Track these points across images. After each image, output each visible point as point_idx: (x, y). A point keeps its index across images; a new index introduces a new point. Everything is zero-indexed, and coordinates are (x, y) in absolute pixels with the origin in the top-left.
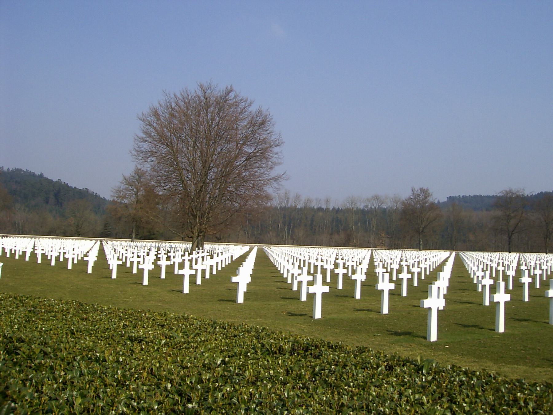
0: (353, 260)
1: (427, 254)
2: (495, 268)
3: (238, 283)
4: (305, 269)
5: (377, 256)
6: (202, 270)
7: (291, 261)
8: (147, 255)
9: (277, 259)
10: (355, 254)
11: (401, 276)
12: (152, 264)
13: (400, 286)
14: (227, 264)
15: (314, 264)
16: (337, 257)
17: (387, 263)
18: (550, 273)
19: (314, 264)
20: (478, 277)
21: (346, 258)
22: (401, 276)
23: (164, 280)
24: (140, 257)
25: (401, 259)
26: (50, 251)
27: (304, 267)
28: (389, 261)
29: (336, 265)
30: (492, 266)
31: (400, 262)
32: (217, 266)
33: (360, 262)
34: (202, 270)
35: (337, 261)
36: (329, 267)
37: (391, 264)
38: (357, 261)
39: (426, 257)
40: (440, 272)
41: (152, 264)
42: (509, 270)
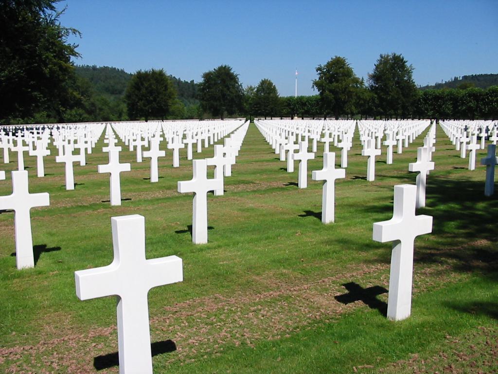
0: (339, 130)
1: (410, 123)
2: (318, 142)
3: (146, 259)
4: (305, 144)
5: (362, 126)
6: (202, 140)
7: (278, 132)
8: (34, 150)
9: (268, 134)
10: (341, 125)
11: (319, 175)
12: (160, 137)
13: (161, 176)
14: (219, 138)
15: (302, 134)
16: (324, 128)
17: (372, 133)
18: (393, 161)
19: (302, 134)
20: (338, 165)
21: (332, 129)
22: (319, 175)
23: (157, 184)
24: (144, 140)
25: (322, 132)
26: (131, 141)
27: (303, 142)
28: (374, 131)
29: (322, 135)
30: (311, 137)
31: (384, 131)
32: (409, 139)
33: (346, 132)
34: (202, 140)
35: (324, 132)
36: (316, 137)
37: (375, 133)
38: (342, 132)
39: (413, 125)
40: (413, 164)
41: (160, 137)
42: (370, 147)
